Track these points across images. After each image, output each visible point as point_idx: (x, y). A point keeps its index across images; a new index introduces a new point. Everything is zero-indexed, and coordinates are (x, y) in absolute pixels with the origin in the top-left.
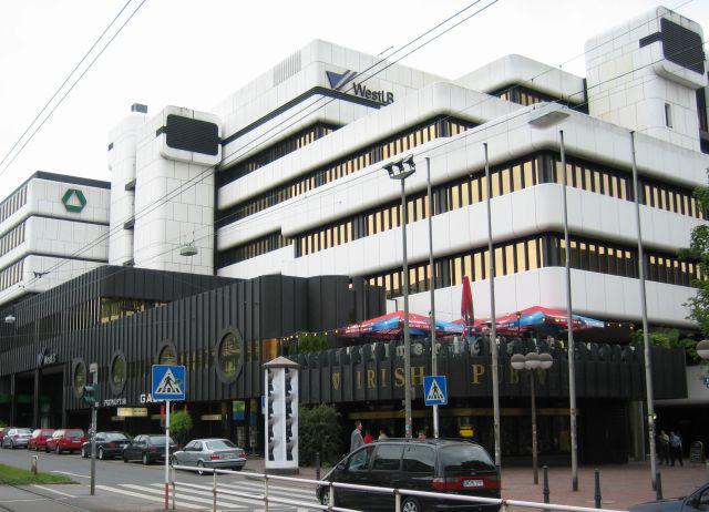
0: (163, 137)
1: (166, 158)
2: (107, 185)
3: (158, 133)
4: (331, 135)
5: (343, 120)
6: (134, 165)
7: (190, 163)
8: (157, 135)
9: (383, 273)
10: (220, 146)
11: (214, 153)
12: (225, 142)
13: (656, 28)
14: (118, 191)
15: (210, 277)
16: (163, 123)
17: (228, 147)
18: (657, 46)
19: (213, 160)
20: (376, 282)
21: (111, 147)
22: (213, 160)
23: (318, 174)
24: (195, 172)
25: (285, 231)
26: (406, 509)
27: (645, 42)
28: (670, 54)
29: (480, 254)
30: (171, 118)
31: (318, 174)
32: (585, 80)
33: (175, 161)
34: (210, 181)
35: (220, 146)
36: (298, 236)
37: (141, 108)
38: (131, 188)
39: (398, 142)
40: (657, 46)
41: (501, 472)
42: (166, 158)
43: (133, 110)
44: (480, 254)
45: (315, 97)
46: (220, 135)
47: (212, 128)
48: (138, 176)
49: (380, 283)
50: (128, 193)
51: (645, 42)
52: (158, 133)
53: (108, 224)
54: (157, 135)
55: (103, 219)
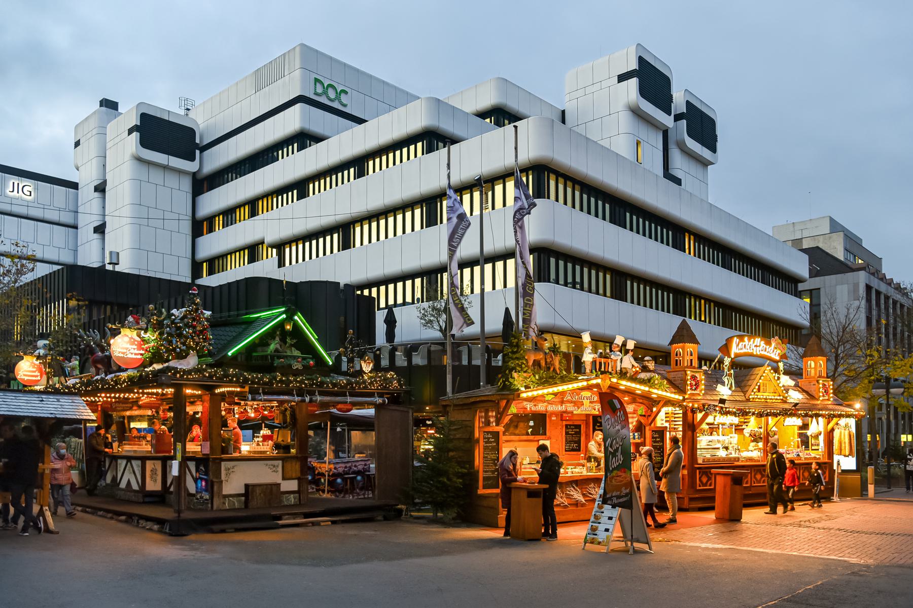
0: (135, 136)
1: (139, 159)
2: (74, 186)
3: (130, 131)
4: (313, 150)
5: (326, 133)
6: (104, 166)
7: (166, 168)
8: (129, 134)
9: (377, 283)
10: (198, 152)
11: (192, 158)
12: (204, 149)
13: (633, 65)
14: (87, 193)
15: (189, 283)
16: (135, 121)
17: (206, 153)
18: (633, 82)
19: (191, 166)
20: (370, 292)
21: (77, 144)
22: (191, 166)
23: (301, 187)
24: (172, 181)
25: (268, 239)
26: (7, 262)
27: (622, 78)
28: (644, 92)
29: (502, 262)
30: (145, 118)
31: (301, 187)
32: (563, 112)
33: (149, 163)
34: (186, 185)
35: (198, 152)
36: (280, 246)
37: (110, 105)
38: (101, 189)
39: (405, 150)
40: (633, 82)
41: (121, 330)
42: (139, 159)
43: (101, 105)
44: (502, 262)
45: (298, 107)
46: (197, 141)
47: (191, 132)
48: (109, 178)
49: (374, 294)
50: (97, 194)
51: (622, 78)
52: (130, 131)
53: (75, 227)
54: (129, 134)
55: (67, 218)
